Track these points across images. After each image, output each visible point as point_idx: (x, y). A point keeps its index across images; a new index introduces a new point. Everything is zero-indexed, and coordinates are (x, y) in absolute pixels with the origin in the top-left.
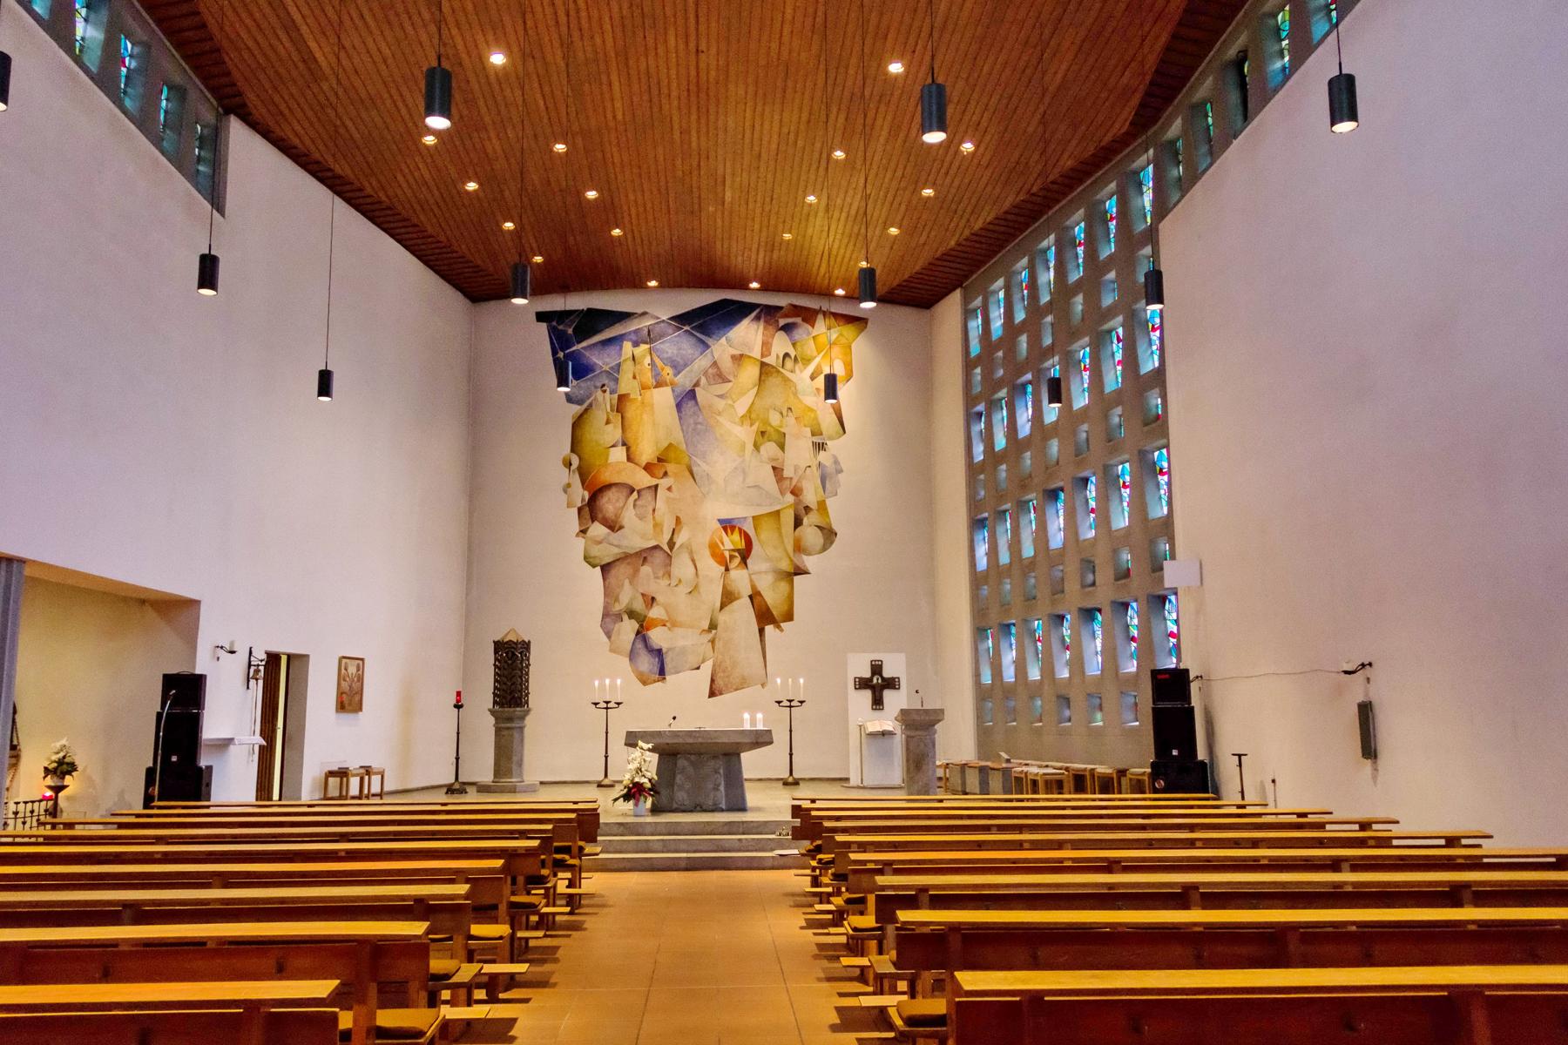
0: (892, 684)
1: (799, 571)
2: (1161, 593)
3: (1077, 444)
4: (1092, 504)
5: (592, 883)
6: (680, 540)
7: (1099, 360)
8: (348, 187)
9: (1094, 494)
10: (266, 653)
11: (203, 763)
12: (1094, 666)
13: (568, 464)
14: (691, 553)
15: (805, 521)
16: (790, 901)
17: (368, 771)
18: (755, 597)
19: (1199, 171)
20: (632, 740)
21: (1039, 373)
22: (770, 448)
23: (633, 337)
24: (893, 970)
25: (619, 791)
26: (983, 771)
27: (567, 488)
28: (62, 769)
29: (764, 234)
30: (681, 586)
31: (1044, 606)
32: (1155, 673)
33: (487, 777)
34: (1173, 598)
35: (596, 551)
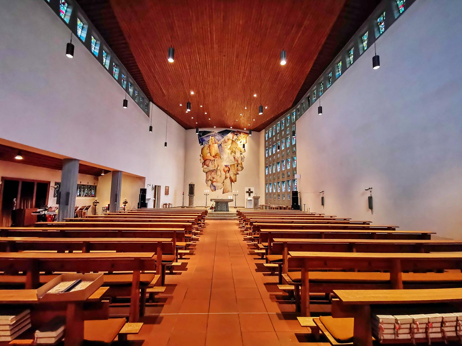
0: (252, 192)
1: (238, 174)
2: (294, 179)
3: (282, 155)
4: (284, 165)
5: (206, 221)
6: (218, 168)
7: (286, 141)
8: (167, 112)
9: (285, 163)
10: (155, 185)
11: (146, 202)
12: (284, 190)
13: (201, 156)
14: (220, 171)
15: (239, 166)
16: (236, 224)
17: (170, 204)
18: (230, 178)
19: (313, 90)
20: (211, 200)
21: (277, 144)
22: (233, 154)
23: (212, 135)
24: (252, 232)
25: (209, 208)
26: (266, 206)
27: (200, 160)
28: (126, 203)
29: (233, 120)
30: (218, 176)
31: (276, 181)
32: (293, 192)
33: (188, 205)
34: (296, 180)
35: (205, 170)
